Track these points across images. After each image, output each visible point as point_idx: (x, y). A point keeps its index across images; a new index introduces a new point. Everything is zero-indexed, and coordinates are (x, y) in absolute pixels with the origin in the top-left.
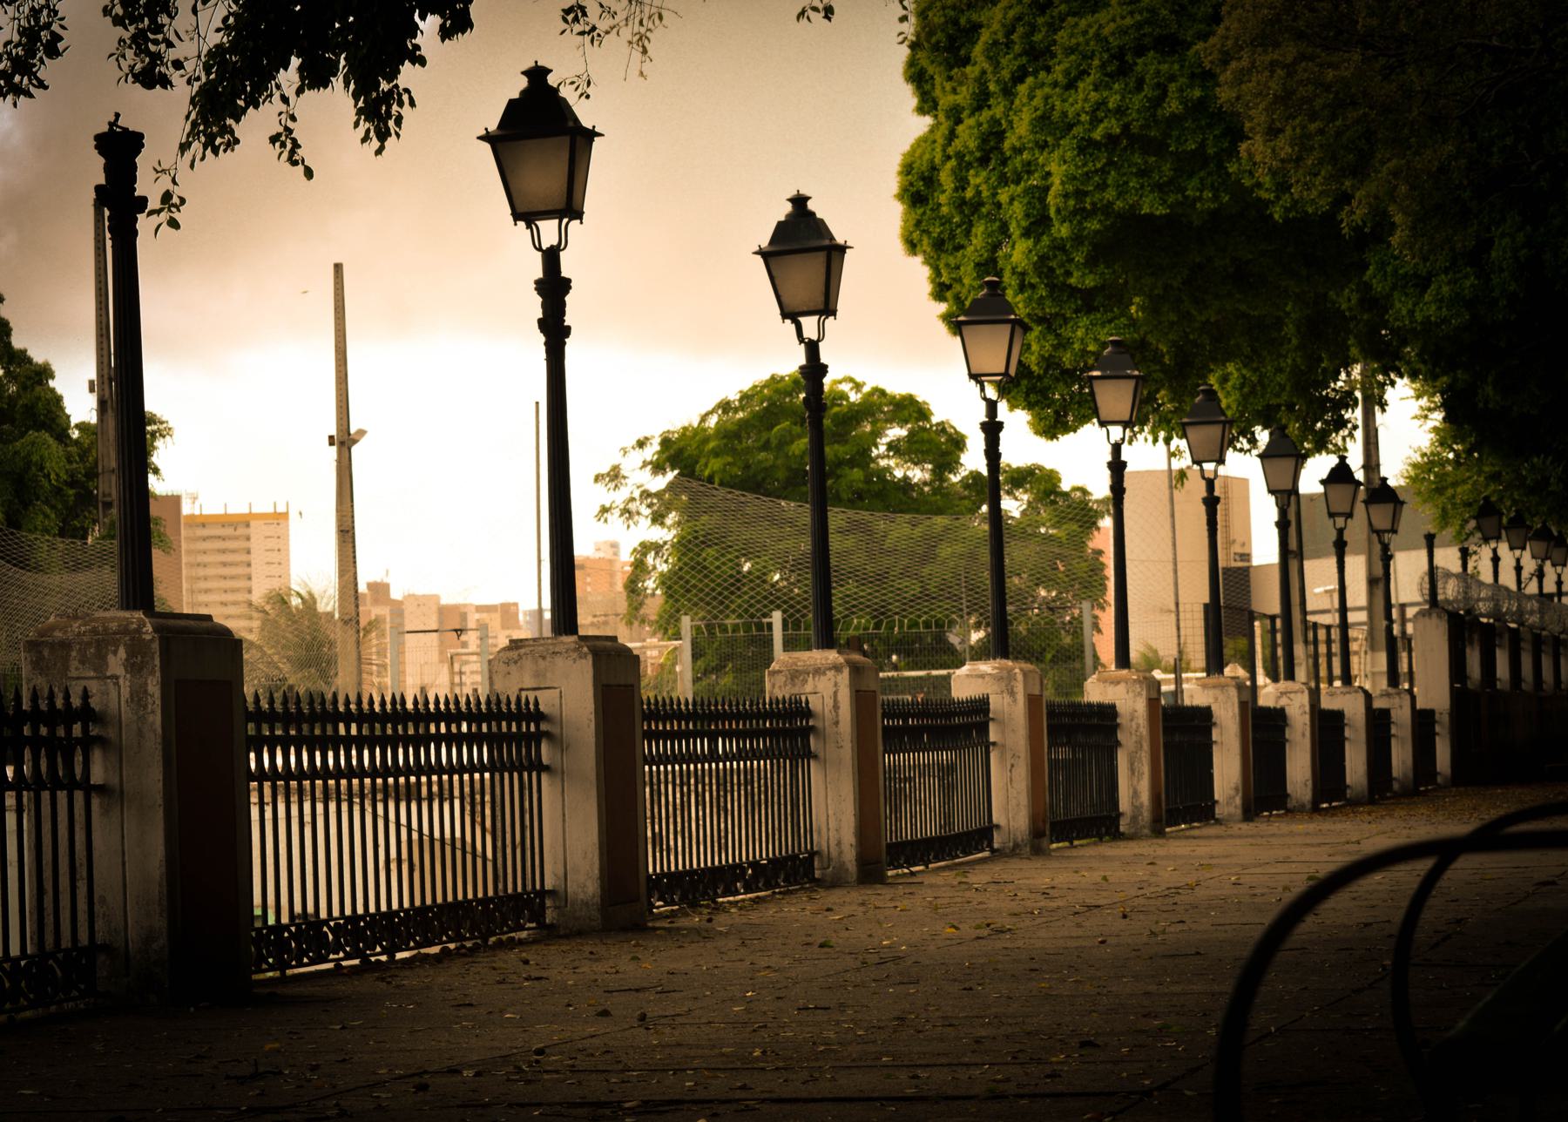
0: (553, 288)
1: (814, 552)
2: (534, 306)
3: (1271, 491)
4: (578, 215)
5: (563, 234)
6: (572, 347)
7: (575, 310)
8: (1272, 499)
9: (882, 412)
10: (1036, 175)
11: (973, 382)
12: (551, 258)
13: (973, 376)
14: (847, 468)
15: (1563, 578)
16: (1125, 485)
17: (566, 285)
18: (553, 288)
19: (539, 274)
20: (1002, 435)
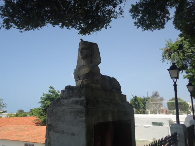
0: (175, 86)
1: (176, 102)
2: (173, 87)
3: (189, 91)
4: (178, 79)
5: (176, 80)
6: (178, 92)
7: (178, 88)
8: (189, 92)
9: (80, 25)
10: (109, 8)
11: (172, 79)
12: (175, 83)
13: (171, 78)
14: (71, 27)
15: (177, 83)
16: (177, 89)
17: (177, 85)
18: (175, 86)
19: (174, 84)
20: (177, 87)
